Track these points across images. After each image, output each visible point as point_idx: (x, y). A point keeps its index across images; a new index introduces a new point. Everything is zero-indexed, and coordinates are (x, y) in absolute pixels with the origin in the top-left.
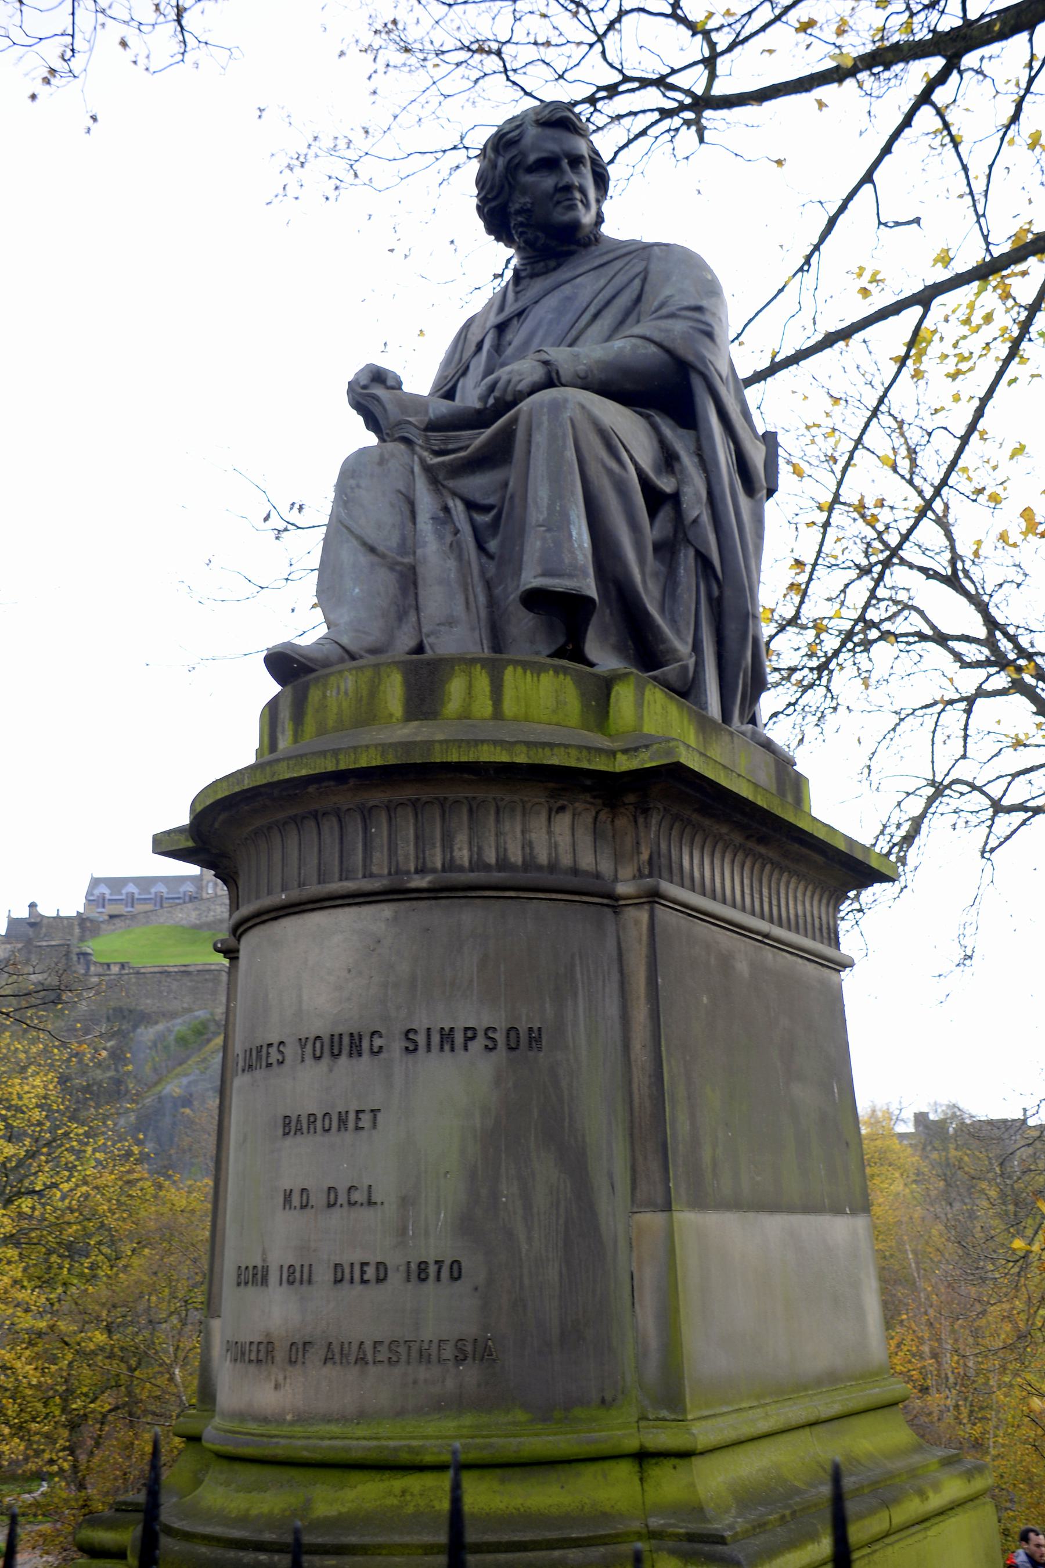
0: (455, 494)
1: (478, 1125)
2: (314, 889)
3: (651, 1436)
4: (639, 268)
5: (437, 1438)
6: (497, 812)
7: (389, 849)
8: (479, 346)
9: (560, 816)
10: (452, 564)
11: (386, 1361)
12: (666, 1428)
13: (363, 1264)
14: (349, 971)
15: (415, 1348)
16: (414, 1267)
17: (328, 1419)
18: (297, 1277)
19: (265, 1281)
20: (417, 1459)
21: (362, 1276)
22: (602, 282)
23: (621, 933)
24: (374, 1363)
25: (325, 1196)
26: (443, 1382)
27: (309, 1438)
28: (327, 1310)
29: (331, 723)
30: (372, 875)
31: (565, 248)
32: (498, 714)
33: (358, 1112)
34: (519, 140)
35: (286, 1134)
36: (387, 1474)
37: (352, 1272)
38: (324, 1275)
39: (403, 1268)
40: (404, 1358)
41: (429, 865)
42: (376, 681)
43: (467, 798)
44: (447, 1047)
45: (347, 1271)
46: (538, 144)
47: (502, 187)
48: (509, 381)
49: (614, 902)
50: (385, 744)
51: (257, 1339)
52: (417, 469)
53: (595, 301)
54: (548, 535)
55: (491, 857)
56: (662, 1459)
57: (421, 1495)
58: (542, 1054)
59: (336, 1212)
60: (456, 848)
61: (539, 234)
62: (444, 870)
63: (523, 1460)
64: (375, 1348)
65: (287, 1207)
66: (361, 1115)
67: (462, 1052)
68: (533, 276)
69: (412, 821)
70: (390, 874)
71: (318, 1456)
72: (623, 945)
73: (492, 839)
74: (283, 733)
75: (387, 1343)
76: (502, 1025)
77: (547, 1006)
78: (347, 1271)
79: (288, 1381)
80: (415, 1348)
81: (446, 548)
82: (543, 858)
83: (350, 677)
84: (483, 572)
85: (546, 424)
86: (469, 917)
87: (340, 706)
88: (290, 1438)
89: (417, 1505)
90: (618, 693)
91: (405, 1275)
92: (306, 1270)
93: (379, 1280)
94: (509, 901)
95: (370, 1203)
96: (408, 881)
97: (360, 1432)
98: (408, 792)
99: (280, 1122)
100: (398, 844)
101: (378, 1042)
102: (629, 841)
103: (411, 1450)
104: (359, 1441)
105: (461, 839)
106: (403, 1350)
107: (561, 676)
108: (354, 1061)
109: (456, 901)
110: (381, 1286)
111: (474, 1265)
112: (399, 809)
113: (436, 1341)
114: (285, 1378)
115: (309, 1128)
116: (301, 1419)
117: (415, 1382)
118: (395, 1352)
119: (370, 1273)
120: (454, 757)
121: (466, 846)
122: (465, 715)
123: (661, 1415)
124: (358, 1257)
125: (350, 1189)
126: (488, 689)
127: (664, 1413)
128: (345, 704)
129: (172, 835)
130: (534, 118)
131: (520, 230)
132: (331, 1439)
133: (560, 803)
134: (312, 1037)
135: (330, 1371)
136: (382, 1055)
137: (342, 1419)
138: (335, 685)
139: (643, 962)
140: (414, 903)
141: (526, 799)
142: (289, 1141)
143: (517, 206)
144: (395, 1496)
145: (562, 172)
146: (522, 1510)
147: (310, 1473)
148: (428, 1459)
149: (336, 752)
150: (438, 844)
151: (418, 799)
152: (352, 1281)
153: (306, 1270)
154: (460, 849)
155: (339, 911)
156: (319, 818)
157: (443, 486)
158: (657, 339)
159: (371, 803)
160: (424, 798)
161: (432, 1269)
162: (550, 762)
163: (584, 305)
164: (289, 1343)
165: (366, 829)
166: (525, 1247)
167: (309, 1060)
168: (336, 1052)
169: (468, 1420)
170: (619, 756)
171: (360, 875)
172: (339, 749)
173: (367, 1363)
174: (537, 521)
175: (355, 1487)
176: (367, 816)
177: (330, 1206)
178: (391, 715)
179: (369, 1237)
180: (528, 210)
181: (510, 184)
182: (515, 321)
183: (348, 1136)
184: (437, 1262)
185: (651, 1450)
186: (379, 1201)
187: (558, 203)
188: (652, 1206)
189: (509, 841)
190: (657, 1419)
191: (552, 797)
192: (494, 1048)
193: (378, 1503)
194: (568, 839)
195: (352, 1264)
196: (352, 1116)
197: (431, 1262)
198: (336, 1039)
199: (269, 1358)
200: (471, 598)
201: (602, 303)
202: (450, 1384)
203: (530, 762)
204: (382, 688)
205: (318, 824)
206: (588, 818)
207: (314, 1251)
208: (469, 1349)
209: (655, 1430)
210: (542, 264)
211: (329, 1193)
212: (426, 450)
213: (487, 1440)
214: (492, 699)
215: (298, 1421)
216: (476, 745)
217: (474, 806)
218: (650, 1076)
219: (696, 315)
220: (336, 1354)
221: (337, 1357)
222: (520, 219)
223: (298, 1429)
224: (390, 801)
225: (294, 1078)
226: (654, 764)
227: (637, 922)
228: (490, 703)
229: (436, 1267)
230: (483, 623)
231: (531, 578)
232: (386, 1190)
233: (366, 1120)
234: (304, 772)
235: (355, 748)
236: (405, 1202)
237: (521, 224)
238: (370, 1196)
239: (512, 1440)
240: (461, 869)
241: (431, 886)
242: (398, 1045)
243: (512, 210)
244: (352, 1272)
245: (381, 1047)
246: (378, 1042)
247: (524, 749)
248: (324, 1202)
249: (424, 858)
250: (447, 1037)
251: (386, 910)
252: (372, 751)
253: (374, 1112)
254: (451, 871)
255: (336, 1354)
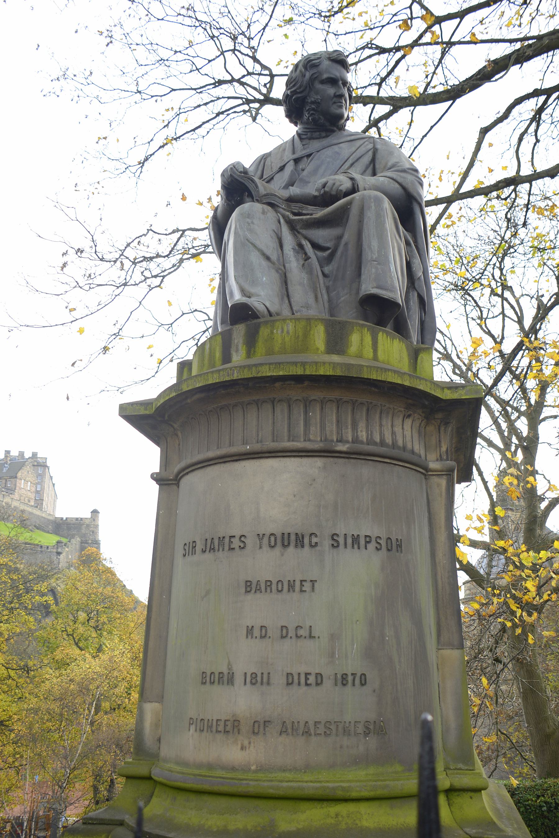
0: (306, 238)
1: (373, 594)
2: (270, 445)
3: (457, 779)
4: (371, 146)
5: (356, 781)
6: (381, 413)
7: (321, 426)
8: (282, 168)
9: (407, 420)
10: (304, 276)
11: (323, 734)
12: (466, 774)
13: (307, 674)
14: (295, 496)
15: (341, 726)
16: (339, 676)
17: (284, 770)
18: (254, 680)
19: (231, 681)
20: (347, 795)
21: (306, 681)
22: (354, 149)
23: (429, 491)
24: (315, 735)
25: (279, 631)
26: (358, 747)
27: (272, 781)
28: (278, 700)
29: (277, 349)
30: (309, 440)
31: (332, 128)
32: (375, 358)
33: (301, 581)
34: (318, 65)
35: (247, 592)
36: (325, 804)
37: (299, 678)
38: (279, 680)
39: (332, 677)
40: (334, 731)
41: (344, 438)
42: (309, 328)
43: (367, 402)
44: (356, 546)
45: (296, 678)
46: (329, 70)
47: (306, 87)
48: (334, 184)
49: (425, 472)
50: (335, 363)
51: (224, 718)
52: (282, 221)
53: (351, 157)
54: (379, 267)
55: (377, 439)
56: (462, 792)
57: (348, 817)
58: (402, 555)
59: (287, 643)
60: (359, 430)
61: (321, 117)
62: (353, 442)
63: (404, 795)
64: (265, 725)
65: (250, 637)
66: (304, 583)
67: (364, 550)
68: (311, 138)
69: (335, 411)
70: (321, 440)
71: (281, 793)
72: (430, 497)
73: (378, 428)
74: (237, 351)
75: (323, 723)
76: (384, 536)
77: (404, 527)
78: (296, 678)
79: (252, 744)
80: (341, 726)
81: (300, 266)
82: (400, 443)
83: (291, 324)
84: (324, 283)
85: (373, 207)
86: (366, 471)
87: (283, 339)
88: (257, 780)
89: (346, 824)
90: (422, 358)
91: (334, 681)
92: (265, 676)
93: (317, 684)
94: (385, 464)
95: (311, 637)
96: (336, 446)
97: (306, 778)
98: (335, 394)
99: (243, 584)
100: (325, 423)
101: (314, 540)
102: (434, 440)
103: (343, 789)
104: (309, 783)
105: (362, 425)
106: (333, 727)
107: (401, 343)
108: (299, 550)
109: (359, 461)
110: (319, 688)
111: (372, 676)
112: (328, 403)
113: (353, 723)
114: (250, 743)
115: (266, 589)
116: (261, 769)
117: (341, 747)
118: (328, 728)
119: (312, 680)
120: (374, 377)
121: (364, 430)
122: (359, 356)
123: (459, 767)
124: (303, 669)
125: (297, 627)
126: (371, 343)
127: (460, 766)
128: (287, 339)
129: (135, 406)
130: (328, 56)
131: (311, 112)
132: (287, 782)
133: (410, 412)
134: (268, 534)
135: (283, 739)
136: (318, 548)
137: (295, 769)
138: (280, 327)
139: (443, 507)
140: (336, 459)
141: (396, 407)
142: (250, 596)
143: (313, 99)
144: (332, 818)
145: (339, 87)
146: (405, 825)
147: (271, 803)
148: (354, 795)
149: (304, 364)
150: (349, 427)
151: (341, 399)
152: (299, 684)
153: (265, 676)
154: (361, 431)
155: (287, 460)
156: (275, 403)
157: (299, 232)
158: (400, 181)
159: (312, 398)
160: (345, 399)
161: (350, 678)
162: (419, 388)
163: (346, 158)
164: (253, 721)
165: (306, 413)
166: (398, 667)
167: (265, 547)
168: (286, 544)
169: (372, 770)
170: (446, 390)
171: (302, 440)
172: (306, 362)
173: (310, 735)
174: (372, 258)
175: (305, 812)
176: (308, 405)
177: (282, 637)
178: (318, 349)
179: (311, 657)
180: (319, 103)
181: (310, 87)
182: (305, 159)
183: (296, 596)
184: (352, 674)
185: (457, 787)
186: (317, 636)
187: (335, 103)
188: (451, 646)
189: (385, 430)
190: (456, 769)
191: (406, 409)
192: (380, 549)
193: (322, 822)
194: (410, 433)
195: (299, 674)
196: (298, 584)
197: (349, 675)
198: (286, 536)
199: (236, 730)
200: (319, 295)
201: (355, 159)
202: (361, 748)
203: (411, 386)
204: (312, 332)
205: (290, 406)
206: (417, 423)
207: (272, 664)
208: (371, 727)
209: (459, 776)
210: (318, 133)
211: (261, 630)
212: (288, 211)
213: (384, 783)
214: (372, 348)
215: (260, 770)
216: (385, 371)
217: (370, 408)
218: (448, 572)
219: (415, 173)
220: (287, 729)
221: (290, 731)
222: (313, 106)
223: (260, 775)
224: (324, 398)
225: (254, 558)
226: (468, 397)
227: (439, 485)
228: (372, 350)
229: (352, 677)
230: (327, 310)
231: (369, 287)
232: (321, 628)
233: (307, 586)
234: (281, 373)
235: (316, 363)
236: (333, 637)
237: (313, 109)
238: (311, 633)
239: (396, 782)
240: (362, 442)
241: (349, 450)
242: (327, 543)
243: (309, 101)
244: (299, 678)
245: (316, 543)
246: (314, 540)
247: (408, 378)
248: (279, 634)
249: (342, 434)
250: (356, 540)
251: (319, 462)
252: (327, 366)
253: (313, 582)
254: (357, 443)
255: (287, 729)
